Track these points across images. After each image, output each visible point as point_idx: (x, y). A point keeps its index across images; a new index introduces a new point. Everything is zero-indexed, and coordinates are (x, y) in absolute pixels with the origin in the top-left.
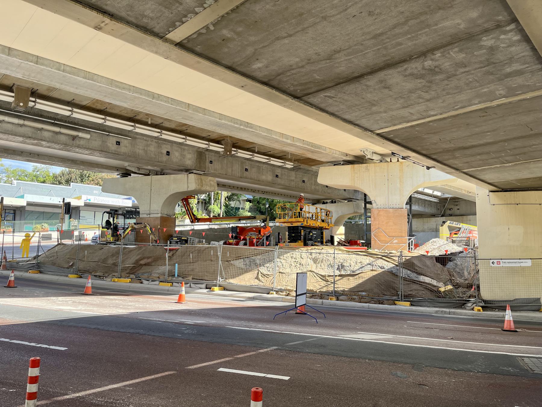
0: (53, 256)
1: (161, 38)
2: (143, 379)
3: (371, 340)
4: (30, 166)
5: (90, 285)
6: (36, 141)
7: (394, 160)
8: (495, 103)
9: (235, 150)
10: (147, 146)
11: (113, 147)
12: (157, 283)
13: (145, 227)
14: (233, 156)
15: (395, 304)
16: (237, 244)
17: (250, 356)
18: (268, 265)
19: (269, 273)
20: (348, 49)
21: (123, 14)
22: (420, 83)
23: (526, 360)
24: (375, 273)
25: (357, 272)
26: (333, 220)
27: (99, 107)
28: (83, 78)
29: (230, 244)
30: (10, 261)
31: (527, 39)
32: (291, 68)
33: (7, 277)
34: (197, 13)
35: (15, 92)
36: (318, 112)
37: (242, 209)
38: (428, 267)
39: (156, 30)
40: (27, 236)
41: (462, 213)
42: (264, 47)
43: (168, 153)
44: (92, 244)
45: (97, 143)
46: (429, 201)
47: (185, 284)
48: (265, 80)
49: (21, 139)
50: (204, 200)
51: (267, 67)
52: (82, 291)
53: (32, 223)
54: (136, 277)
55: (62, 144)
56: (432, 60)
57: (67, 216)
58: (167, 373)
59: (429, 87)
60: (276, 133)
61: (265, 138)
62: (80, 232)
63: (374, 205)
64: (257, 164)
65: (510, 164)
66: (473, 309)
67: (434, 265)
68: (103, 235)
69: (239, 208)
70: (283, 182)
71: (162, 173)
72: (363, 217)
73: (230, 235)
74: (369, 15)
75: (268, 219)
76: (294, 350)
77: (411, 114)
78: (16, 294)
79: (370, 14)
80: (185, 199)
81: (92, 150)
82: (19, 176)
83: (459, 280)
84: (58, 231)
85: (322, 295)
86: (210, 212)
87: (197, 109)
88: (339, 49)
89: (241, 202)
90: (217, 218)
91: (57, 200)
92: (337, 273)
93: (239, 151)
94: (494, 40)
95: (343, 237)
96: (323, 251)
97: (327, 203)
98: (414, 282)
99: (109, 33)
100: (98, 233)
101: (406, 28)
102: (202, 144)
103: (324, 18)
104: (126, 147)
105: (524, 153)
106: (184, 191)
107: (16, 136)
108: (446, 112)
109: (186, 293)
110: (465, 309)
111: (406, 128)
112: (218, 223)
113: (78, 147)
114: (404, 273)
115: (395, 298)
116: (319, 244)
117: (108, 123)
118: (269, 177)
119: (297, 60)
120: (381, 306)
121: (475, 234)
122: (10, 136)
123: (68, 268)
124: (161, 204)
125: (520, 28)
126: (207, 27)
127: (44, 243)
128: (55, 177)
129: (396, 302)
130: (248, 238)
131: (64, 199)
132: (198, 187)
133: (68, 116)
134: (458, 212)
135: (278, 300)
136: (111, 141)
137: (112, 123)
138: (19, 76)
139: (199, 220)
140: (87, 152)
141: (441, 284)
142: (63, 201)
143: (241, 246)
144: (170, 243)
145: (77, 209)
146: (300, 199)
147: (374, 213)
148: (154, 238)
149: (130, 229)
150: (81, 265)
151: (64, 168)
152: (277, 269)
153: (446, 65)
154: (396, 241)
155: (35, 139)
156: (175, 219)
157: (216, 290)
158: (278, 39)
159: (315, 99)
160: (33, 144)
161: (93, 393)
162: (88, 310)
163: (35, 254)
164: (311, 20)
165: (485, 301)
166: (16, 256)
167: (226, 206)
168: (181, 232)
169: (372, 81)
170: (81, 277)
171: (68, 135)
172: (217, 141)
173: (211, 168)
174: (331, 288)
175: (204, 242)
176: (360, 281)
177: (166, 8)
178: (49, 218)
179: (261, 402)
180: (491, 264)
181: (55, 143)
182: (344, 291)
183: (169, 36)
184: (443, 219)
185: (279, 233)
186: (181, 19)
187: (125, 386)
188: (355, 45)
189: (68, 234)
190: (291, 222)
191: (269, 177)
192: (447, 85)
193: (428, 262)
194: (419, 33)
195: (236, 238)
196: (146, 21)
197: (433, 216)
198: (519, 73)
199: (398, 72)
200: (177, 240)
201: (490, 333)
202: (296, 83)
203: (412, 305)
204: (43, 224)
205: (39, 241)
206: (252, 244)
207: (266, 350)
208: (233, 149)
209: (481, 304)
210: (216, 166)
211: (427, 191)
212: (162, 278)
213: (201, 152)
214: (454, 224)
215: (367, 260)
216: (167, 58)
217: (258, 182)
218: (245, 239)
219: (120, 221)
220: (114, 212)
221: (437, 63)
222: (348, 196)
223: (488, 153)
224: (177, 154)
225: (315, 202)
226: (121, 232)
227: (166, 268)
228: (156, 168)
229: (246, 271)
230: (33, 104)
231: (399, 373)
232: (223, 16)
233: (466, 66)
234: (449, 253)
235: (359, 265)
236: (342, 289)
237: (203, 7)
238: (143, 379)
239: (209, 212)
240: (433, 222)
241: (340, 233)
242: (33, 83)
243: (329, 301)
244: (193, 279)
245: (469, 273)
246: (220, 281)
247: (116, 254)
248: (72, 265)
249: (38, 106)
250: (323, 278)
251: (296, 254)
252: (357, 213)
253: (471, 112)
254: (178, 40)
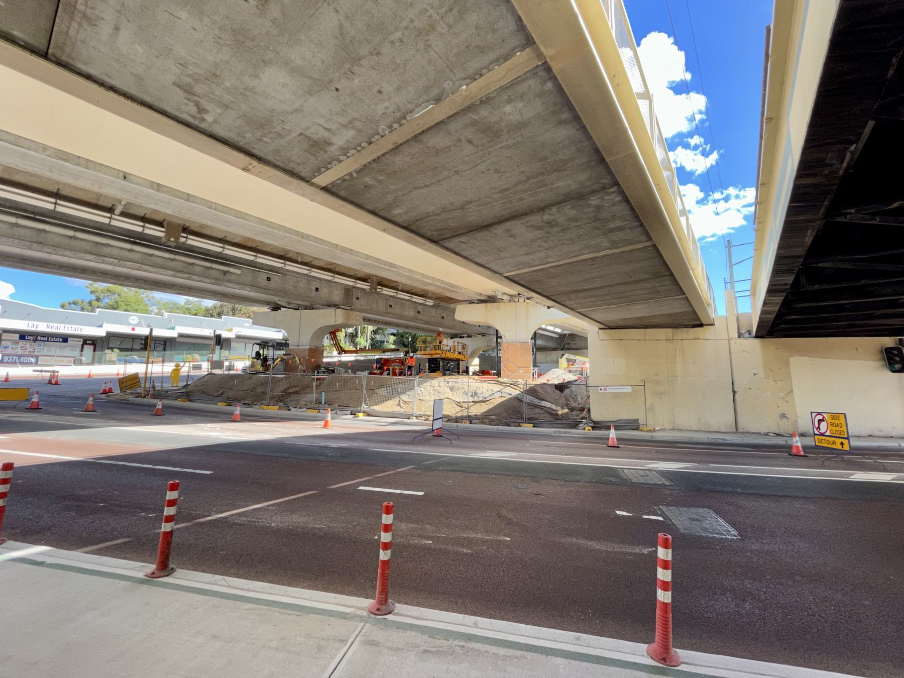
0: (203, 385)
1: (307, 182)
2: (286, 499)
4: (182, 299)
5: (238, 412)
6: (187, 276)
7: (521, 300)
8: (601, 254)
9: (380, 287)
10: (298, 282)
11: (264, 282)
12: (304, 410)
13: (294, 358)
14: (378, 293)
15: (520, 426)
16: (381, 374)
17: (389, 475)
18: (408, 393)
19: (410, 400)
20: (478, 200)
21: (270, 158)
22: (539, 233)
23: (626, 471)
24: (503, 399)
25: (488, 399)
26: (469, 352)
27: (250, 244)
28: (235, 217)
29: (375, 374)
30: (158, 390)
31: (626, 200)
32: (428, 215)
33: (155, 406)
34: (341, 161)
35: (165, 226)
36: (453, 255)
37: (387, 342)
38: (548, 393)
39: (302, 174)
40: (177, 366)
41: (579, 347)
42: (403, 195)
43: (317, 289)
44: (242, 373)
45: (248, 278)
46: (551, 337)
47: (331, 410)
48: (405, 225)
49: (171, 273)
50: (352, 333)
51: (406, 213)
52: (229, 418)
53: (182, 354)
55: (214, 279)
56: (549, 214)
57: (218, 348)
58: (309, 493)
59: (548, 237)
60: (417, 273)
61: (407, 277)
62: (230, 362)
63: (504, 339)
64: (401, 301)
65: (614, 306)
66: (584, 429)
67: (554, 392)
68: (253, 365)
69: (384, 341)
70: (424, 318)
71: (311, 308)
72: (495, 350)
73: (374, 366)
74: (495, 172)
75: (410, 351)
76: (429, 468)
77: (533, 260)
78: (163, 421)
79: (497, 171)
80: (333, 334)
81: (243, 285)
82: (171, 308)
83: (574, 405)
84: (208, 361)
85: (457, 420)
86: (357, 344)
87: (344, 250)
88: (470, 200)
89: (386, 335)
90: (363, 350)
91: (208, 332)
92: (471, 399)
93: (384, 288)
94: (600, 200)
95: (477, 368)
96: (459, 380)
97: (464, 337)
98: (537, 406)
99: (257, 175)
100: (248, 363)
101: (527, 185)
102: (349, 282)
103: (457, 172)
104: (276, 282)
105: (625, 297)
107: (167, 269)
108: (562, 260)
109: (332, 418)
110: (578, 429)
111: (530, 272)
112: (364, 354)
113: (229, 281)
114: (528, 398)
115: (520, 420)
116: (456, 374)
117: (259, 260)
118: (411, 313)
119: (434, 208)
120: (508, 428)
121: (588, 365)
122: (160, 269)
123: (217, 396)
124: (310, 336)
125: (621, 190)
126: (350, 174)
127: (194, 373)
128: (207, 310)
129: (521, 424)
130: (391, 368)
131: (215, 331)
132: (345, 321)
133: (220, 253)
134: (574, 346)
136: (262, 277)
137: (263, 260)
138: (169, 212)
139: (346, 352)
140: (238, 287)
141: (559, 408)
142: (214, 333)
143: (385, 375)
144: (318, 373)
145: (228, 341)
146: (439, 334)
147: (503, 347)
148: (302, 369)
149: (279, 359)
150: (231, 394)
151: (216, 302)
152: (417, 396)
153: (561, 219)
155: (186, 273)
156: (323, 351)
157: (361, 415)
158: (416, 188)
159: (451, 244)
160: (184, 278)
161: (236, 514)
162: (236, 436)
163: (185, 384)
164: (445, 173)
165: (594, 422)
166: (165, 385)
167: (372, 339)
168: (329, 363)
169: (499, 230)
170: (230, 405)
171: (220, 270)
172: (364, 280)
173: (358, 304)
174: (465, 413)
175: (350, 372)
176: (491, 406)
177: (312, 154)
178: (200, 350)
179: (392, 515)
180: (599, 391)
181: (207, 277)
182: (476, 415)
183: (314, 181)
184: (562, 352)
185: (420, 364)
186: (326, 166)
187: (268, 506)
188: (485, 198)
189: (217, 364)
190: (431, 354)
191: (411, 313)
192: (562, 236)
193: (549, 390)
194: (538, 190)
195: (380, 368)
196: (293, 166)
197: (555, 349)
198: (621, 229)
199: (521, 223)
201: (597, 449)
202: (433, 229)
203: (534, 426)
204: (194, 355)
205: (189, 370)
206: (394, 374)
207: (403, 469)
208: (378, 287)
209: (591, 425)
210: (362, 303)
211: (549, 328)
212: (309, 406)
213: (349, 289)
214: (572, 357)
215: (497, 388)
216: (313, 201)
217: (401, 317)
218: (388, 370)
219: (269, 353)
220: (264, 343)
221: (553, 218)
222: (482, 332)
223: (597, 296)
224: (325, 290)
225: (453, 336)
226: (270, 362)
227: (314, 396)
228: (305, 303)
229: (389, 399)
230: (185, 239)
231: (520, 486)
232: (365, 165)
233: (577, 221)
234: (566, 381)
235: (490, 392)
236: (475, 414)
237: (347, 156)
238: (286, 499)
239: (355, 345)
240: (554, 355)
241: (475, 364)
242: (185, 220)
243: (463, 424)
244: (339, 406)
245: (582, 399)
246: (364, 407)
247: (265, 383)
248: (222, 394)
249: (190, 242)
250: (459, 404)
251: (435, 382)
252: (490, 346)
253: (582, 260)
254: (323, 185)
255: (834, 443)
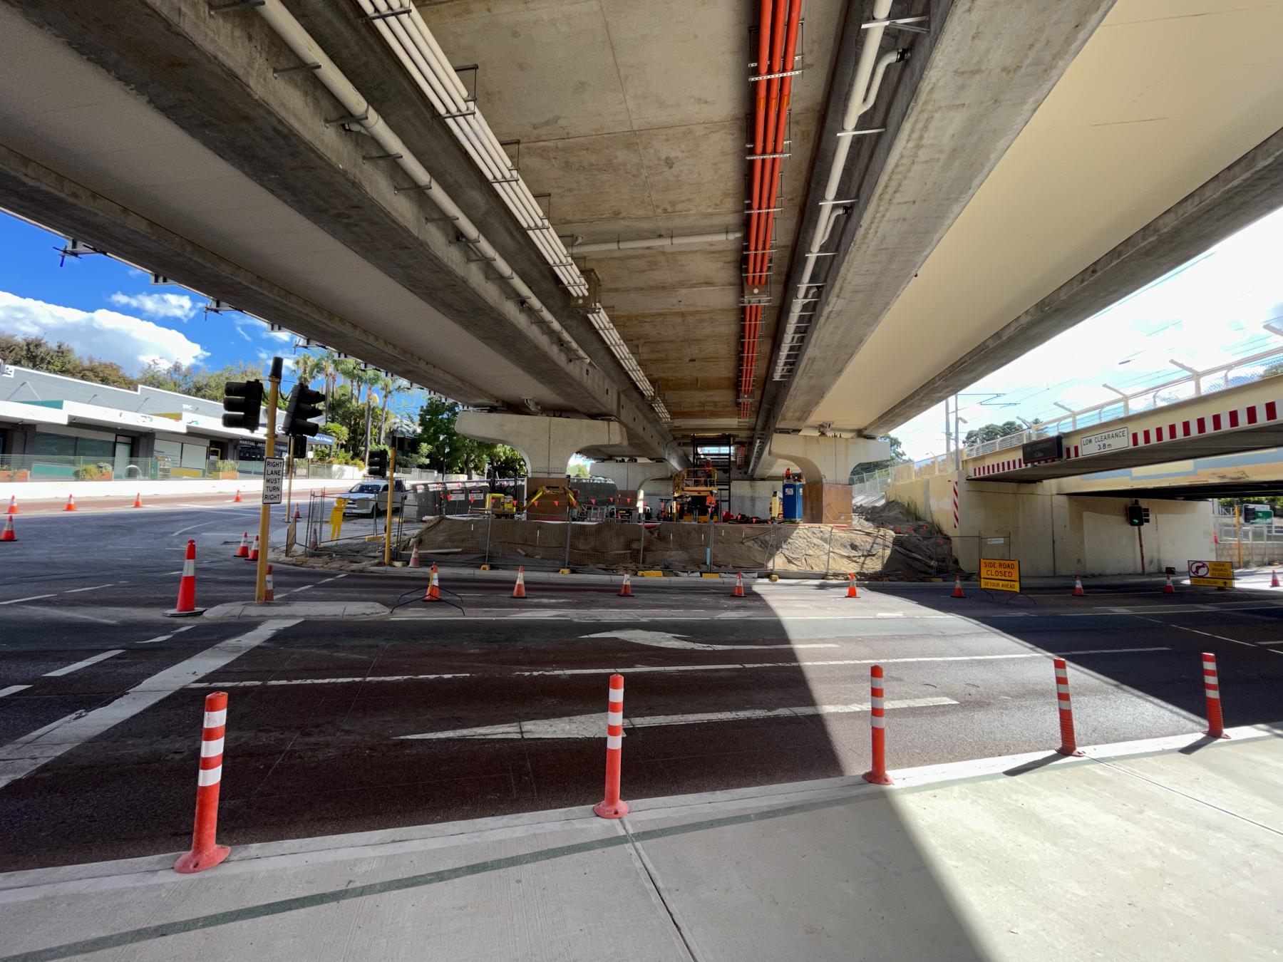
5: (520, 581)
13: (566, 493)
204: (101, 464)
255: (998, 585)
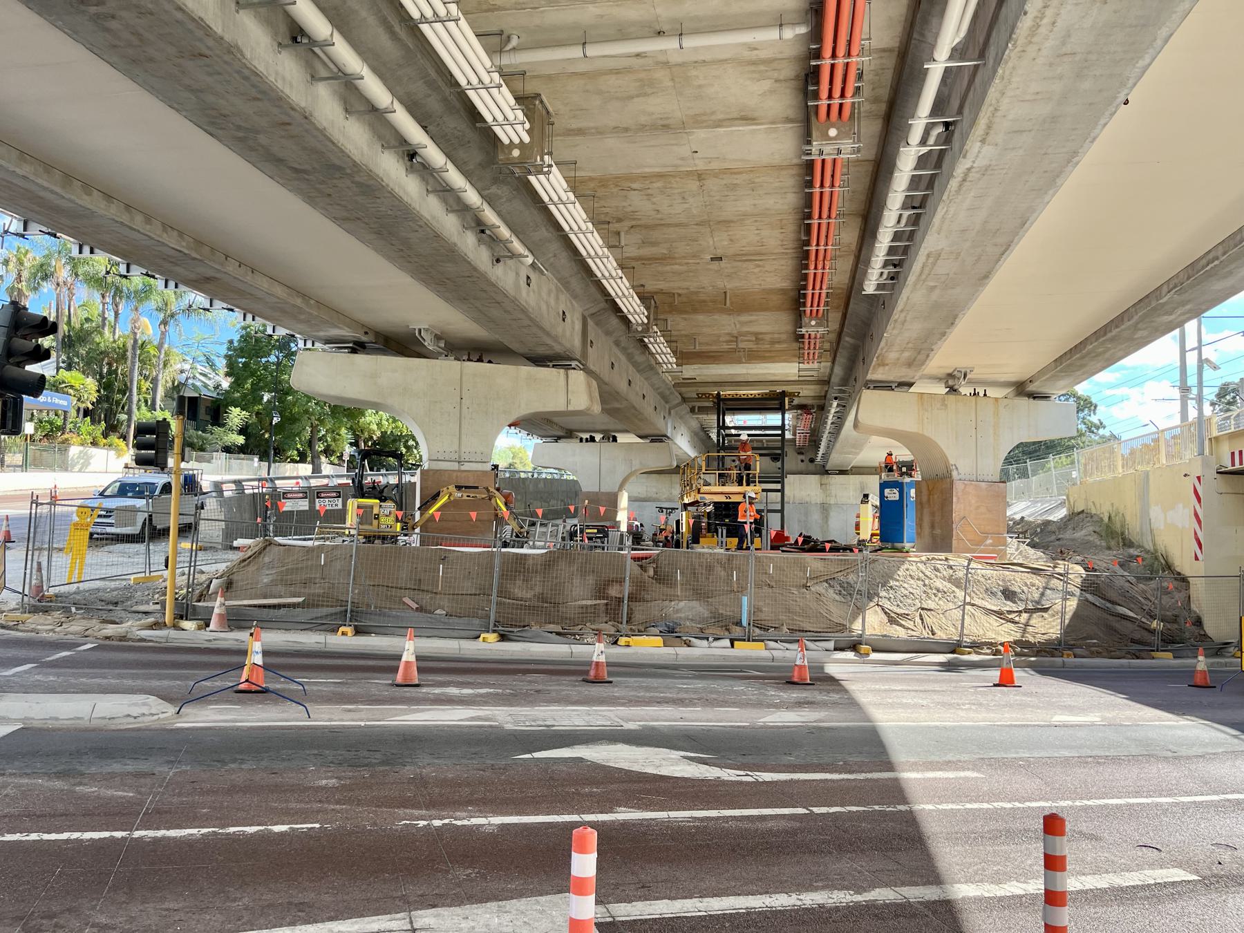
3: (458, 721)
54: (661, 632)
106: (558, 409)
135: (993, 664)
154: (991, 541)
200: (598, 533)
